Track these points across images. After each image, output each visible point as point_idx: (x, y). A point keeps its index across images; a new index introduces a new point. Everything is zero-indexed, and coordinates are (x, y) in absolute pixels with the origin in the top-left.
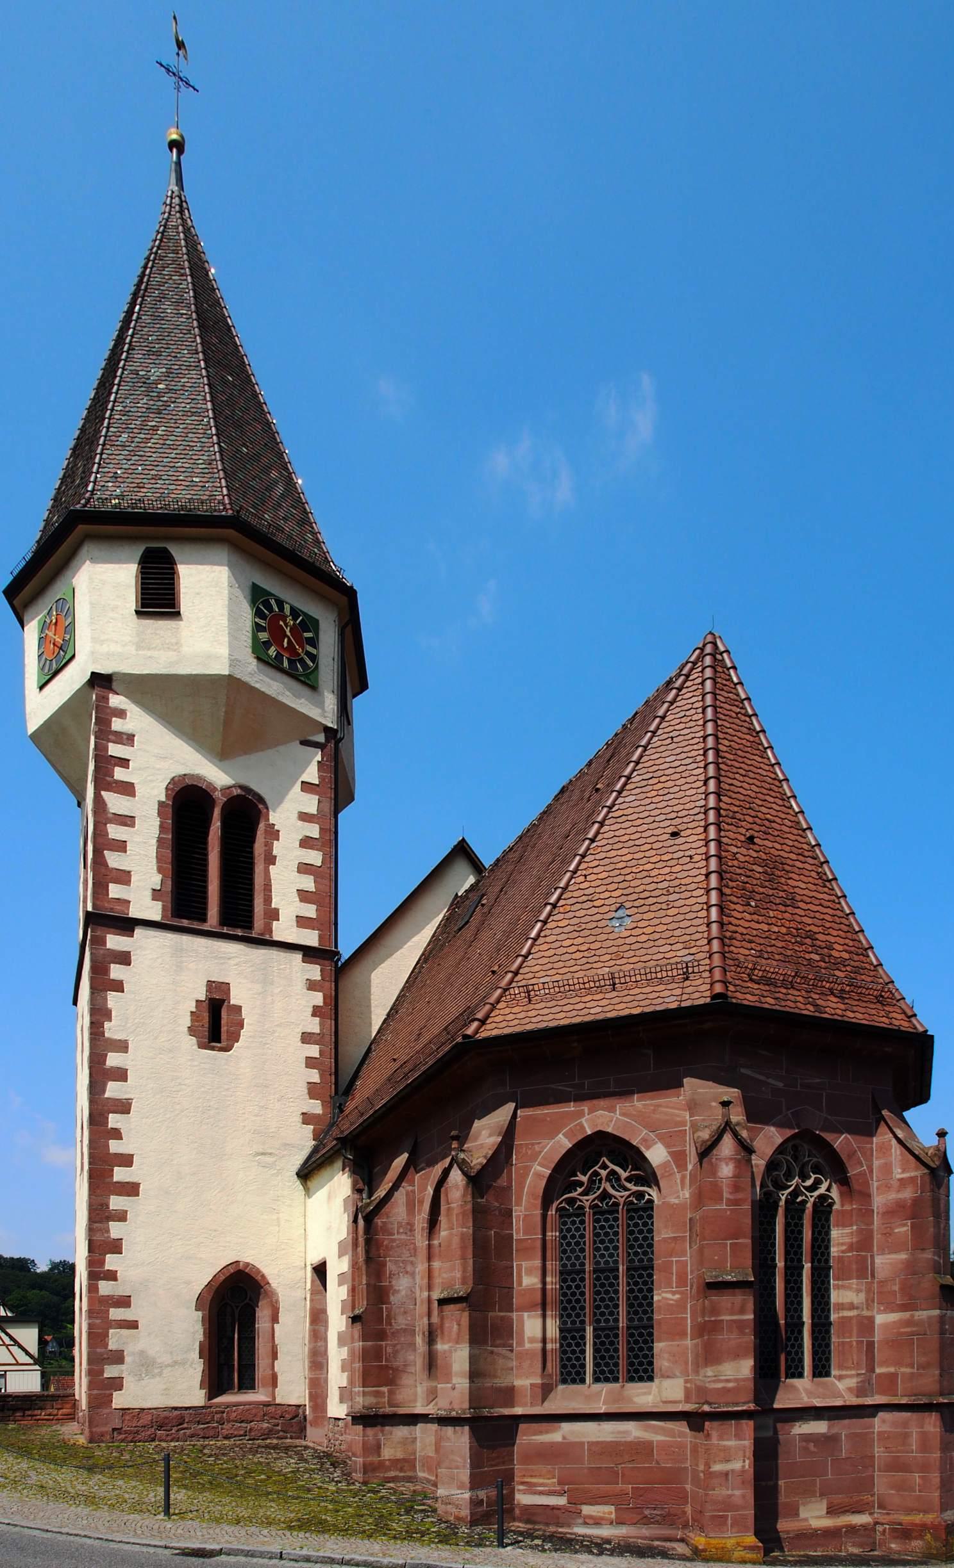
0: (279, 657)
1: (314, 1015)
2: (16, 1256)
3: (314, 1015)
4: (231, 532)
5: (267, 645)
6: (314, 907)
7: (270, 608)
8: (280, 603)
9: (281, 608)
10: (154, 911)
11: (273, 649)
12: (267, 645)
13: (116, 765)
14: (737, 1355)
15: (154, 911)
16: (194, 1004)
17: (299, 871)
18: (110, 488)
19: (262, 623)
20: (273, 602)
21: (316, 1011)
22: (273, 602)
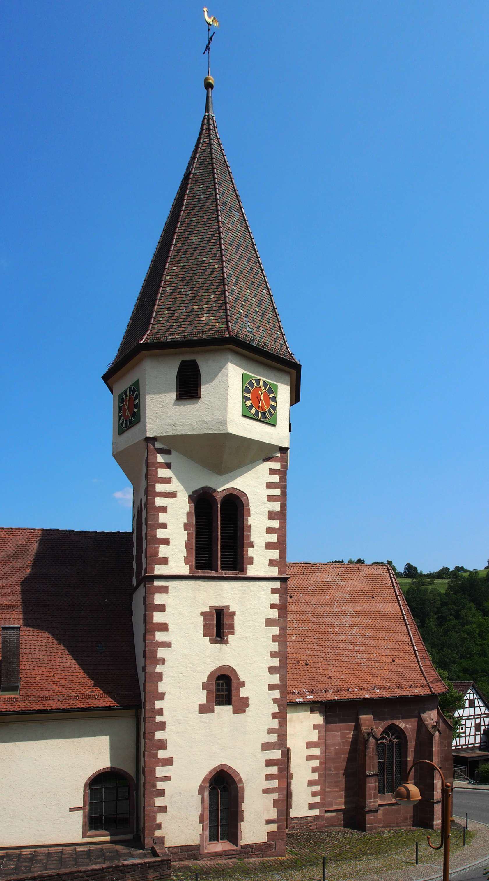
0: (257, 412)
1: (274, 641)
2: (99, 530)
3: (274, 641)
4: (231, 346)
5: (251, 407)
6: (278, 676)
7: (252, 386)
8: (258, 381)
9: (258, 384)
10: (185, 570)
11: (254, 408)
12: (251, 407)
13: (159, 647)
14: (436, 825)
15: (185, 570)
16: (209, 608)
17: (270, 673)
18: (160, 326)
19: (248, 395)
20: (254, 381)
21: (275, 639)
22: (254, 381)
